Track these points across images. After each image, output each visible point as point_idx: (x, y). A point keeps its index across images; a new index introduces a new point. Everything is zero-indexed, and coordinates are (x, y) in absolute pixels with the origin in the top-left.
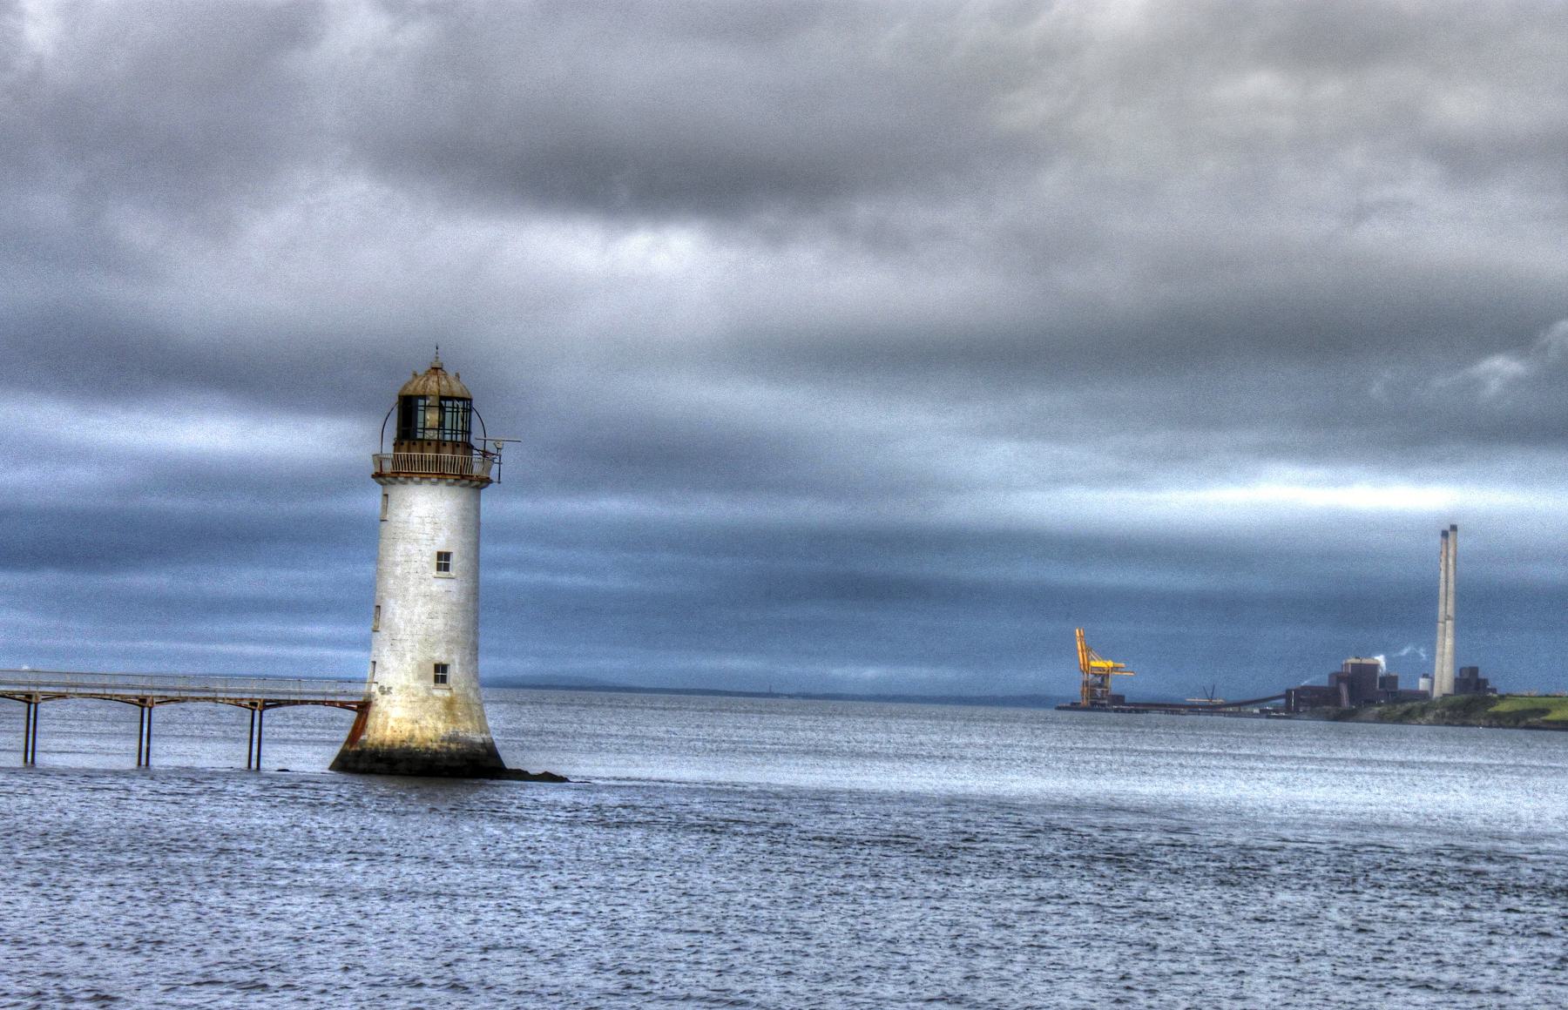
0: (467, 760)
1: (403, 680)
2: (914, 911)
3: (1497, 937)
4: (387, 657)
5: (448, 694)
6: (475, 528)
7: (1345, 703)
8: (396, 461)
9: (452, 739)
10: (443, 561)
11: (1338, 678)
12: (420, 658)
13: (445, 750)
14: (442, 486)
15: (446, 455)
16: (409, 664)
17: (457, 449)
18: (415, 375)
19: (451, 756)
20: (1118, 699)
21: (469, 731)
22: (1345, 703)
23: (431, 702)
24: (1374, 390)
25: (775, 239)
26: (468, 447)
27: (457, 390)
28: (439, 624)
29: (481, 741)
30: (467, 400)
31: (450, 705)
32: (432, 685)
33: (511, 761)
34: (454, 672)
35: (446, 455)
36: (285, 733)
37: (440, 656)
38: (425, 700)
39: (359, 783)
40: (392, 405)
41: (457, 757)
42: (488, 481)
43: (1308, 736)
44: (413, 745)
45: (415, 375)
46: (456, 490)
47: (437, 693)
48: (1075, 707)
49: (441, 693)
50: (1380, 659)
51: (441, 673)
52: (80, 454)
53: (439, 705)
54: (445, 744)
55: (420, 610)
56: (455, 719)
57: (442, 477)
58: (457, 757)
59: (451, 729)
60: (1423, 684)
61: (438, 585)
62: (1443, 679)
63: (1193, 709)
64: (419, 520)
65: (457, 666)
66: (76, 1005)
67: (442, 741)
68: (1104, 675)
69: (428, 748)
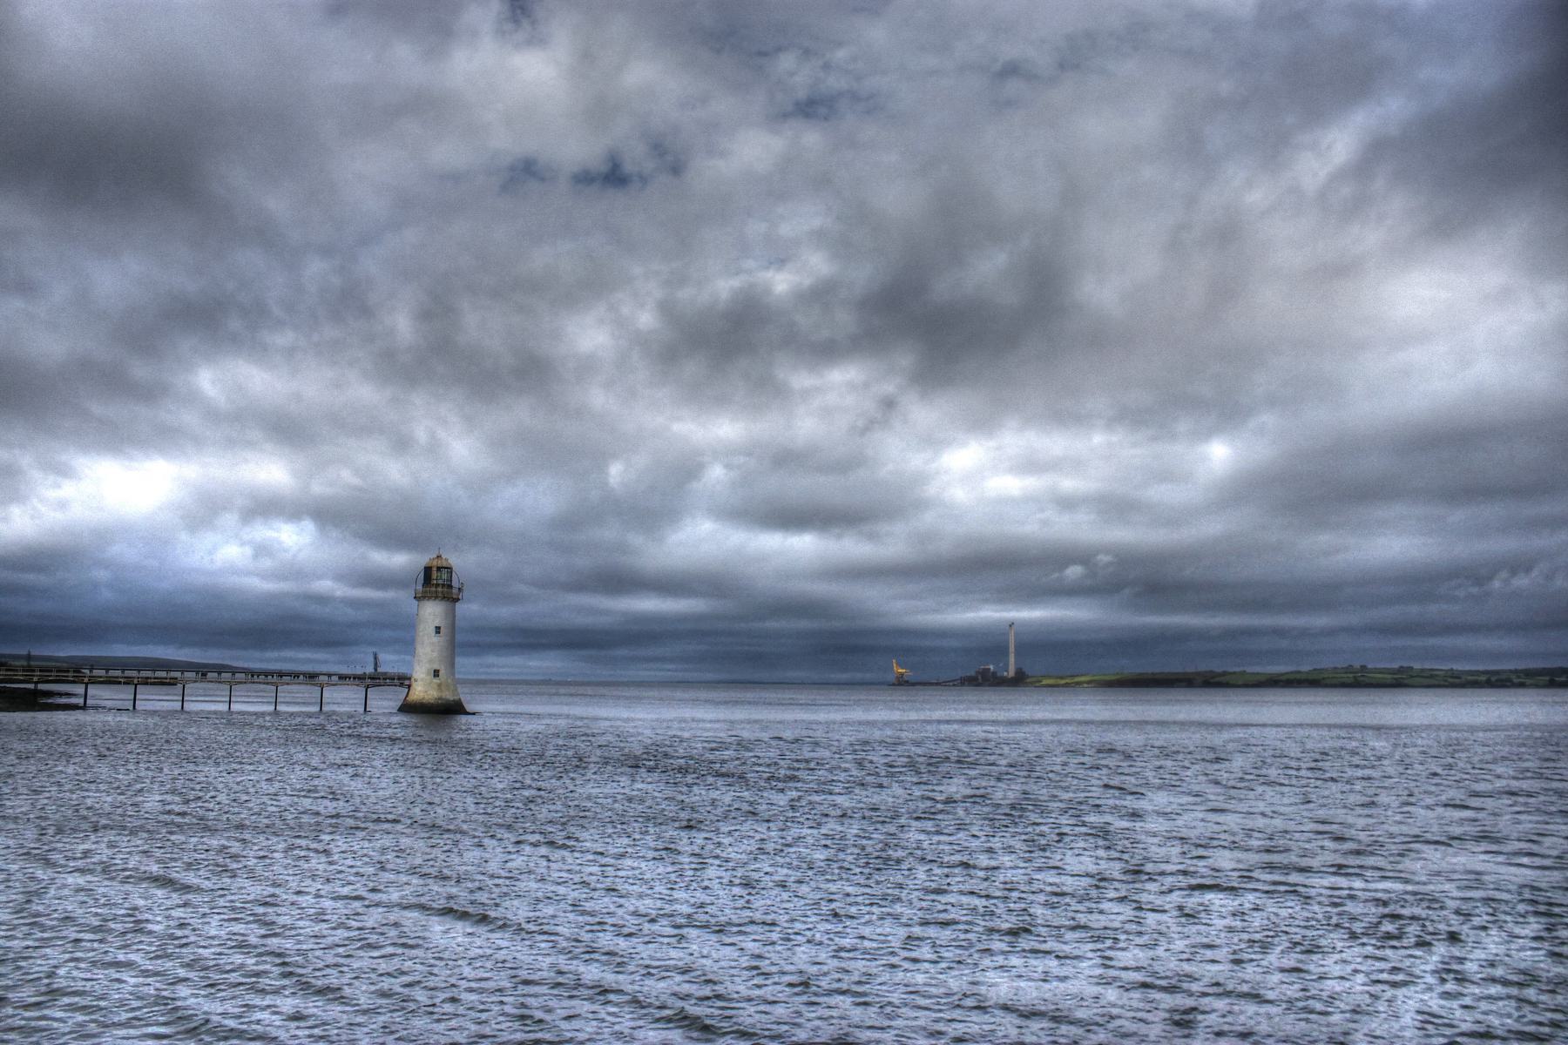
1: (422, 676)
2: (1335, 749)
4: (417, 668)
6: (452, 615)
7: (980, 681)
10: (438, 630)
11: (978, 672)
14: (437, 601)
15: (440, 589)
16: (424, 669)
19: (442, 705)
20: (907, 682)
21: (449, 696)
22: (980, 681)
25: (839, 537)
26: (450, 586)
27: (445, 565)
28: (435, 654)
30: (450, 568)
31: (439, 685)
33: (469, 708)
35: (440, 589)
36: (237, 694)
37: (436, 667)
42: (458, 600)
43: (971, 694)
46: (443, 603)
48: (894, 685)
49: (436, 681)
50: (991, 667)
51: (436, 673)
52: (607, 612)
53: (435, 686)
55: (428, 649)
56: (442, 691)
60: (1005, 674)
61: (435, 639)
62: (1011, 673)
63: (931, 684)
68: (902, 674)
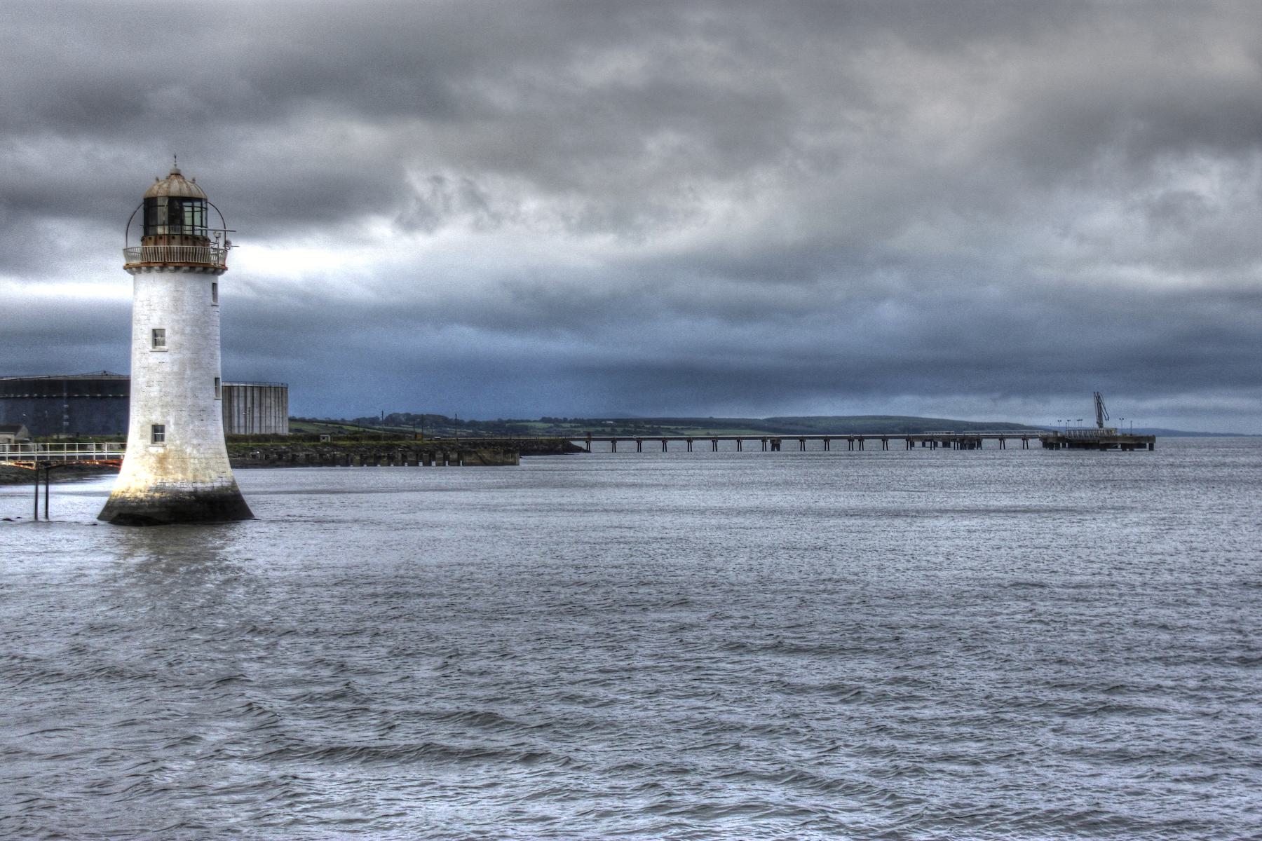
0: (166, 507)
3: (873, 667)
5: (161, 451)
8: (144, 253)
9: (157, 490)
12: (142, 419)
13: (149, 498)
17: (172, 240)
18: (157, 180)
19: (152, 503)
23: (147, 457)
24: (65, 243)
29: (192, 490)
32: (150, 444)
34: (170, 430)
38: (143, 457)
39: (121, 533)
40: (138, 205)
41: (157, 504)
44: (128, 495)
45: (157, 180)
47: (153, 450)
49: (158, 450)
53: (152, 460)
54: (151, 493)
56: (165, 471)
57: (163, 267)
58: (157, 504)
59: (159, 481)
64: (141, 304)
65: (173, 426)
66: (267, 834)
67: (149, 491)
69: (136, 498)
